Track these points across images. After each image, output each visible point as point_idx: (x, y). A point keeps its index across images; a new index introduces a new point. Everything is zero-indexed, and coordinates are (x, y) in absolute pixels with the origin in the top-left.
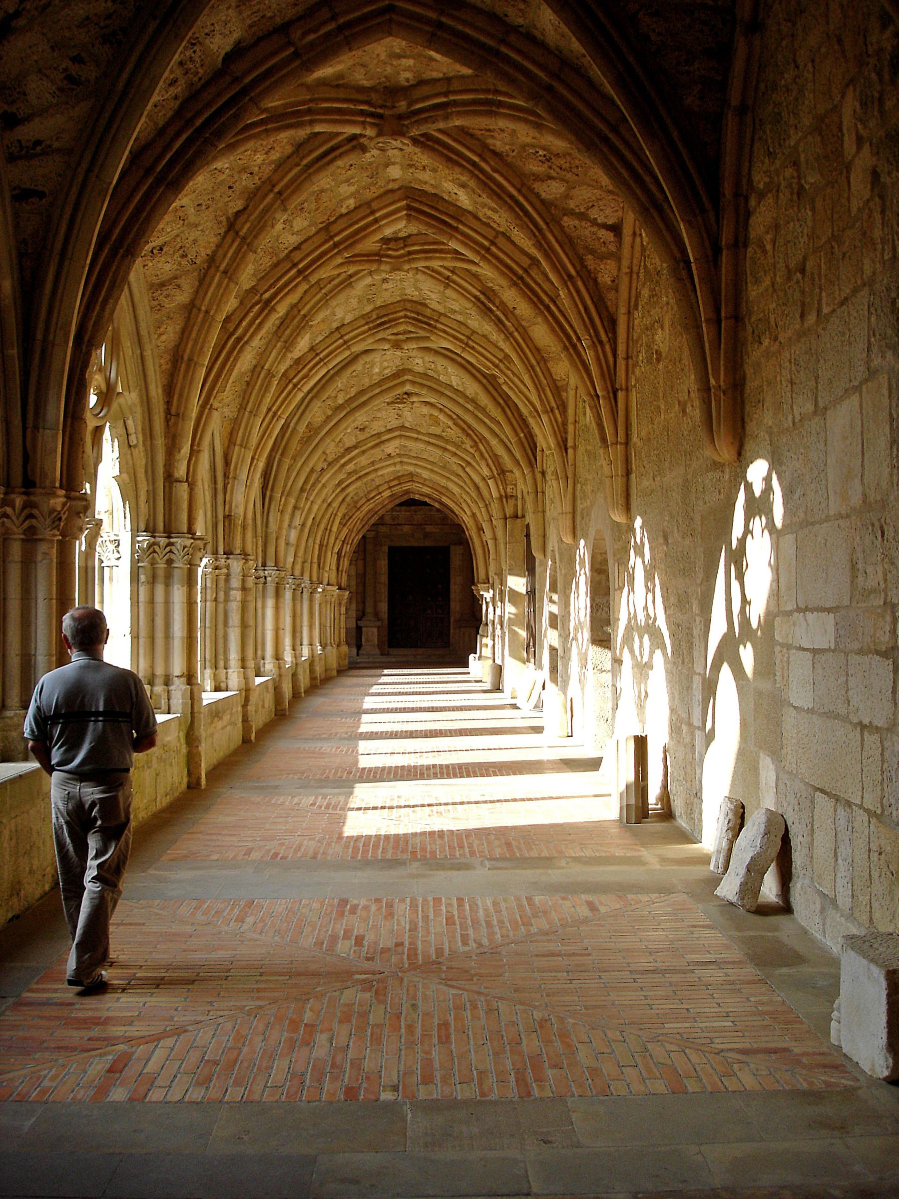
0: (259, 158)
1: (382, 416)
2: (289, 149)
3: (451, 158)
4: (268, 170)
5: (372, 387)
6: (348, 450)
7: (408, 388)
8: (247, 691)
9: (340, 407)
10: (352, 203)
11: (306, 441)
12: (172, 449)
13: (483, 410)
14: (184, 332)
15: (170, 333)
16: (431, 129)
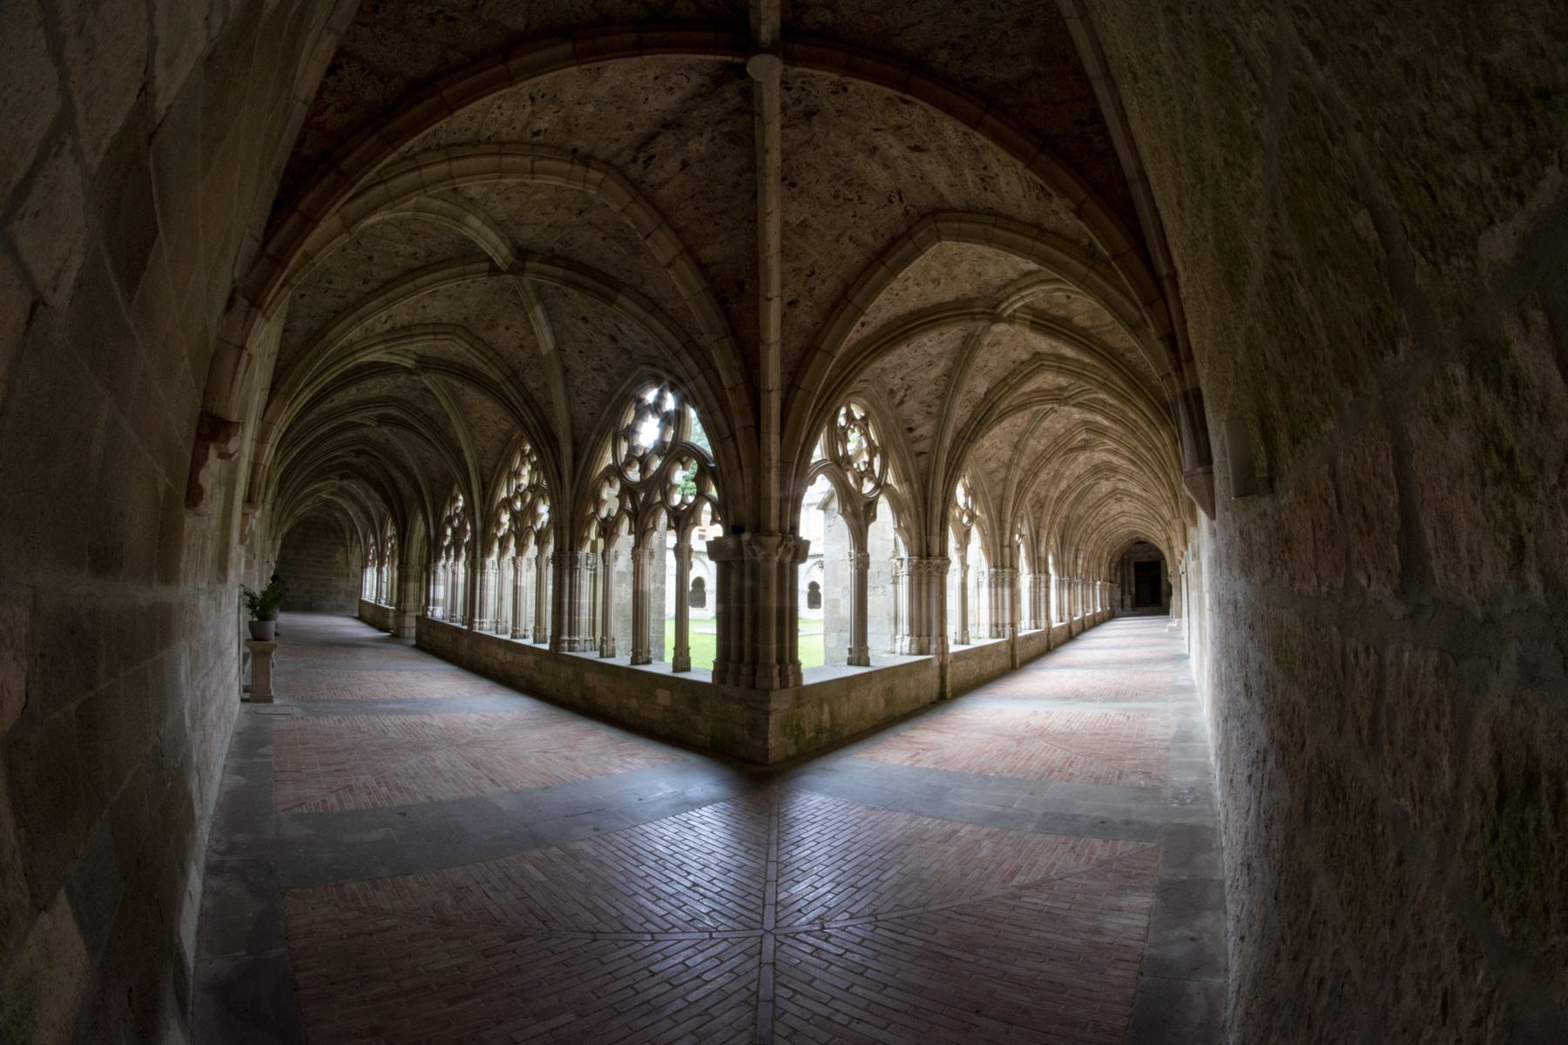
3: (1091, 409)
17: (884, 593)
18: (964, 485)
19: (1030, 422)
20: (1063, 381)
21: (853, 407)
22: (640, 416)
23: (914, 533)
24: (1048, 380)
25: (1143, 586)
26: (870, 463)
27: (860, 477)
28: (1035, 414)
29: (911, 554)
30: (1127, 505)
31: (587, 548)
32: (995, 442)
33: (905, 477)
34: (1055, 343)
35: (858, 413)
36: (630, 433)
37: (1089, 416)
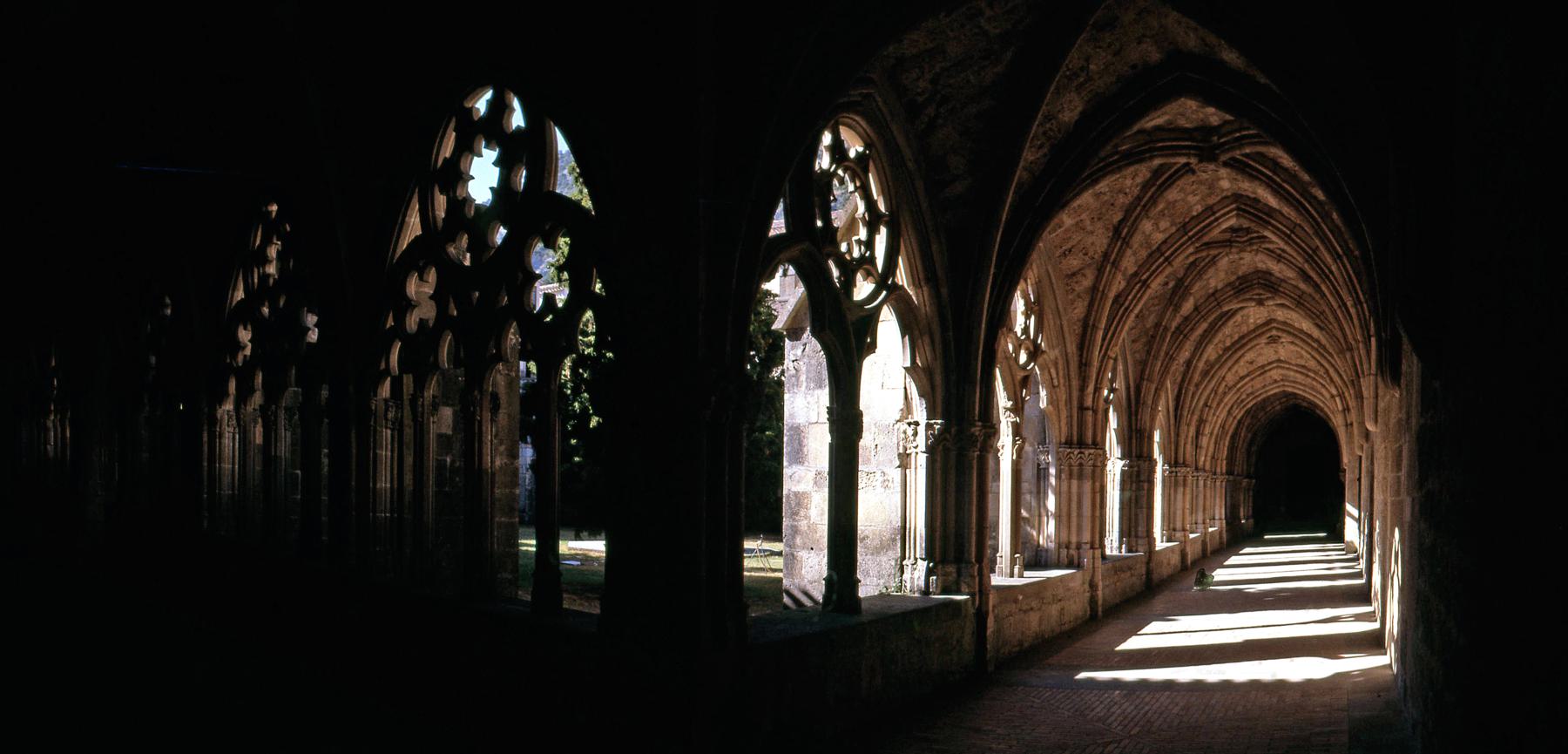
0: (1129, 182)
1: (1262, 353)
2: (1148, 175)
3: (1253, 176)
4: (1136, 191)
5: (1250, 332)
6: (1242, 378)
7: (1274, 332)
8: (1184, 543)
9: (1228, 349)
10: (1199, 208)
11: (1205, 373)
12: (1082, 389)
13: (1324, 348)
14: (1091, 305)
15: (1080, 310)
16: (1237, 154)
17: (886, 484)
18: (1026, 297)
19: (1145, 186)
20: (1214, 116)
21: (845, 133)
22: (466, 148)
23: (938, 379)
24: (1189, 111)
25: (1287, 481)
26: (869, 244)
27: (849, 269)
28: (1157, 173)
29: (931, 414)
30: (1286, 349)
31: (385, 390)
32: (1080, 223)
33: (926, 274)
34: (1212, 39)
35: (855, 148)
36: (455, 175)
37: (1247, 187)
